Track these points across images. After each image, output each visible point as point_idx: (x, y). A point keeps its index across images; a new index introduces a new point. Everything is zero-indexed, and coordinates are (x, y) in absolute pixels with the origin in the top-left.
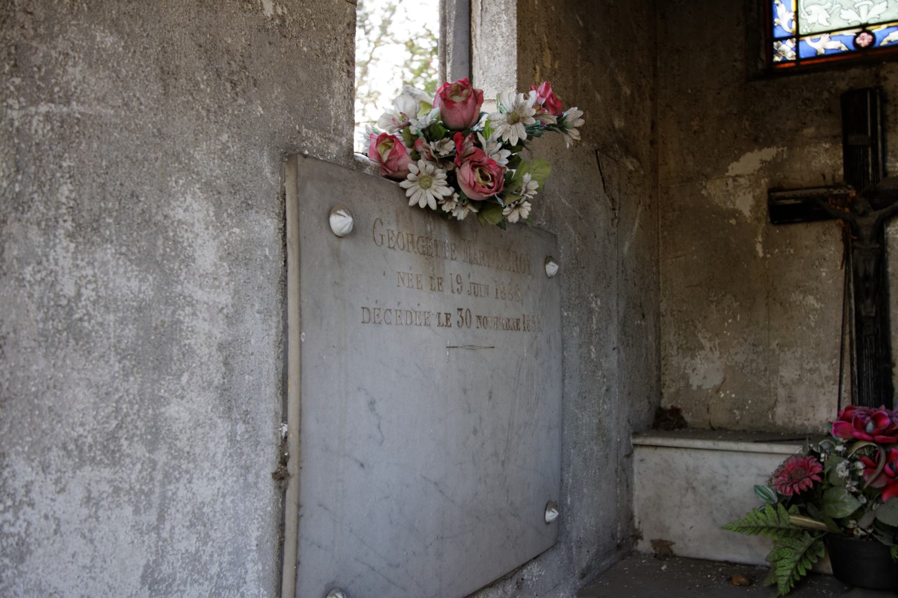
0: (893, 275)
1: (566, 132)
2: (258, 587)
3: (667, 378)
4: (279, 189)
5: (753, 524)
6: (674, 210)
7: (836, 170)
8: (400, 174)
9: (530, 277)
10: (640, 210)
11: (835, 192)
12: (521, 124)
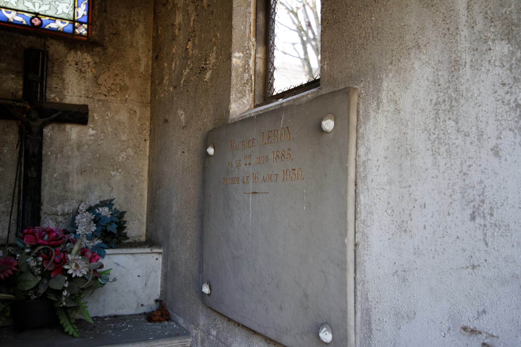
0: (45, 155)
11: (18, 104)
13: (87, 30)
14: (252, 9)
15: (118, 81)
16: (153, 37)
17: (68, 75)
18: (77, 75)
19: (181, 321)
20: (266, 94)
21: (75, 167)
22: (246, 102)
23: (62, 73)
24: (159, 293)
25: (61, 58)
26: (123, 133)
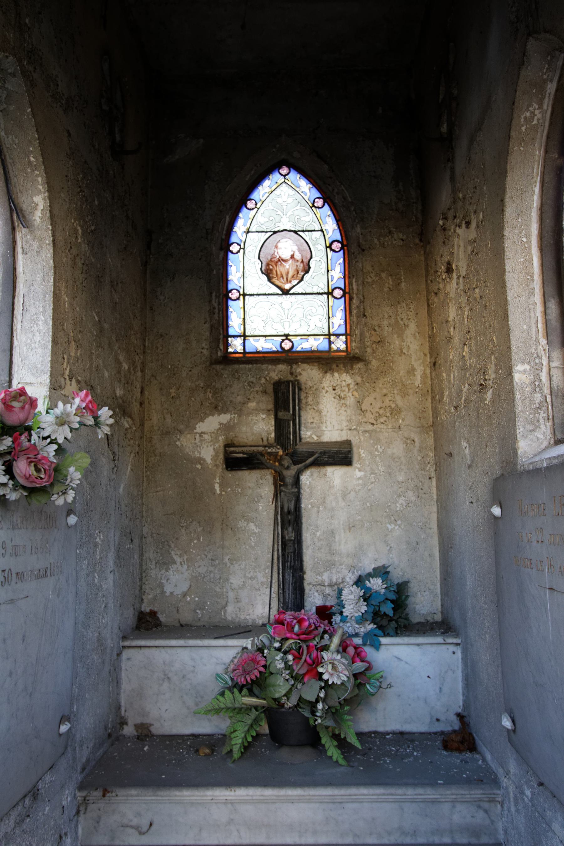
1: (99, 428)
3: (147, 587)
5: (217, 707)
6: (156, 456)
9: (56, 530)
10: (132, 457)
11: (269, 450)
12: (66, 426)
13: (346, 342)
14: (538, 298)
15: (387, 403)
16: (429, 337)
17: (325, 404)
18: (335, 404)
19: (488, 757)
21: (341, 523)
22: (540, 436)
23: (318, 403)
24: (461, 704)
25: (315, 384)
26: (399, 471)
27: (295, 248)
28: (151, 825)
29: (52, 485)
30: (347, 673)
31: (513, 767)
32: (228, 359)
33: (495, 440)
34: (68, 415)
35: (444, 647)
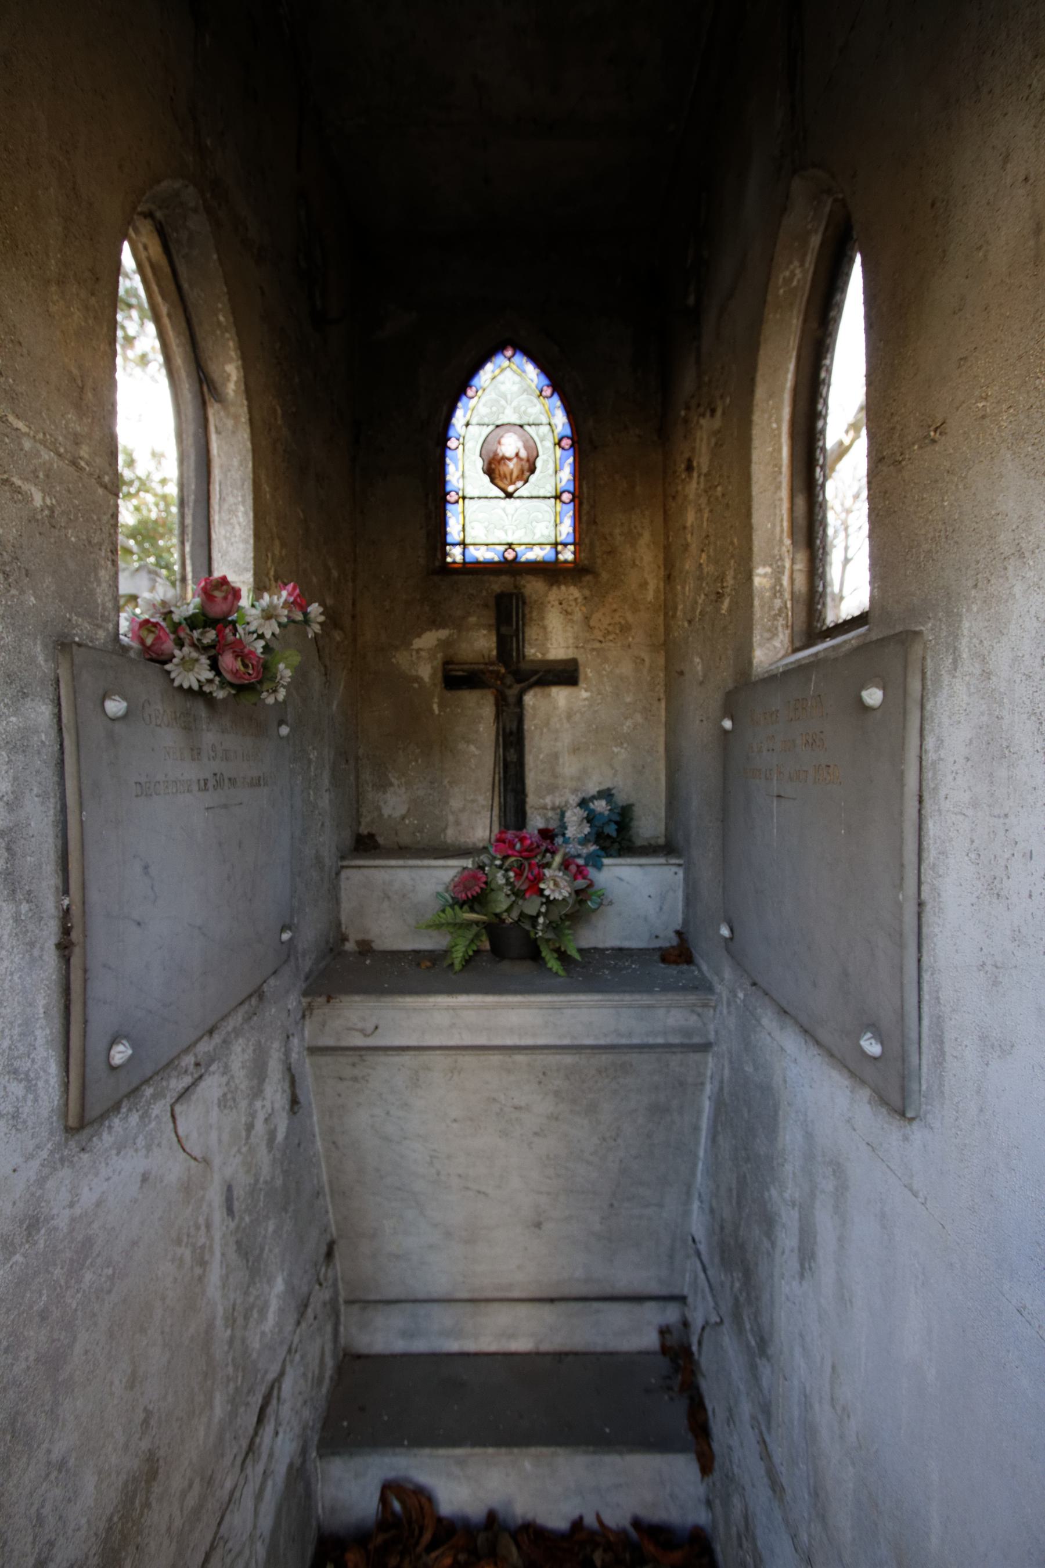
2: (47, 1050)
4: (52, 676)
7: (491, 651)
8: (163, 658)
11: (491, 668)
13: (574, 553)
14: (784, 493)
15: (617, 619)
19: (705, 968)
20: (812, 625)
23: (542, 619)
27: (520, 445)
28: (376, 1028)
29: (260, 682)
30: (569, 889)
31: (728, 973)
32: (448, 570)
33: (730, 652)
34: (275, 607)
35: (667, 868)
